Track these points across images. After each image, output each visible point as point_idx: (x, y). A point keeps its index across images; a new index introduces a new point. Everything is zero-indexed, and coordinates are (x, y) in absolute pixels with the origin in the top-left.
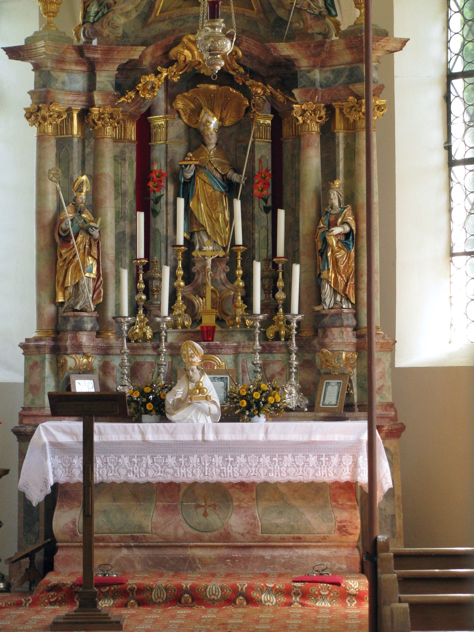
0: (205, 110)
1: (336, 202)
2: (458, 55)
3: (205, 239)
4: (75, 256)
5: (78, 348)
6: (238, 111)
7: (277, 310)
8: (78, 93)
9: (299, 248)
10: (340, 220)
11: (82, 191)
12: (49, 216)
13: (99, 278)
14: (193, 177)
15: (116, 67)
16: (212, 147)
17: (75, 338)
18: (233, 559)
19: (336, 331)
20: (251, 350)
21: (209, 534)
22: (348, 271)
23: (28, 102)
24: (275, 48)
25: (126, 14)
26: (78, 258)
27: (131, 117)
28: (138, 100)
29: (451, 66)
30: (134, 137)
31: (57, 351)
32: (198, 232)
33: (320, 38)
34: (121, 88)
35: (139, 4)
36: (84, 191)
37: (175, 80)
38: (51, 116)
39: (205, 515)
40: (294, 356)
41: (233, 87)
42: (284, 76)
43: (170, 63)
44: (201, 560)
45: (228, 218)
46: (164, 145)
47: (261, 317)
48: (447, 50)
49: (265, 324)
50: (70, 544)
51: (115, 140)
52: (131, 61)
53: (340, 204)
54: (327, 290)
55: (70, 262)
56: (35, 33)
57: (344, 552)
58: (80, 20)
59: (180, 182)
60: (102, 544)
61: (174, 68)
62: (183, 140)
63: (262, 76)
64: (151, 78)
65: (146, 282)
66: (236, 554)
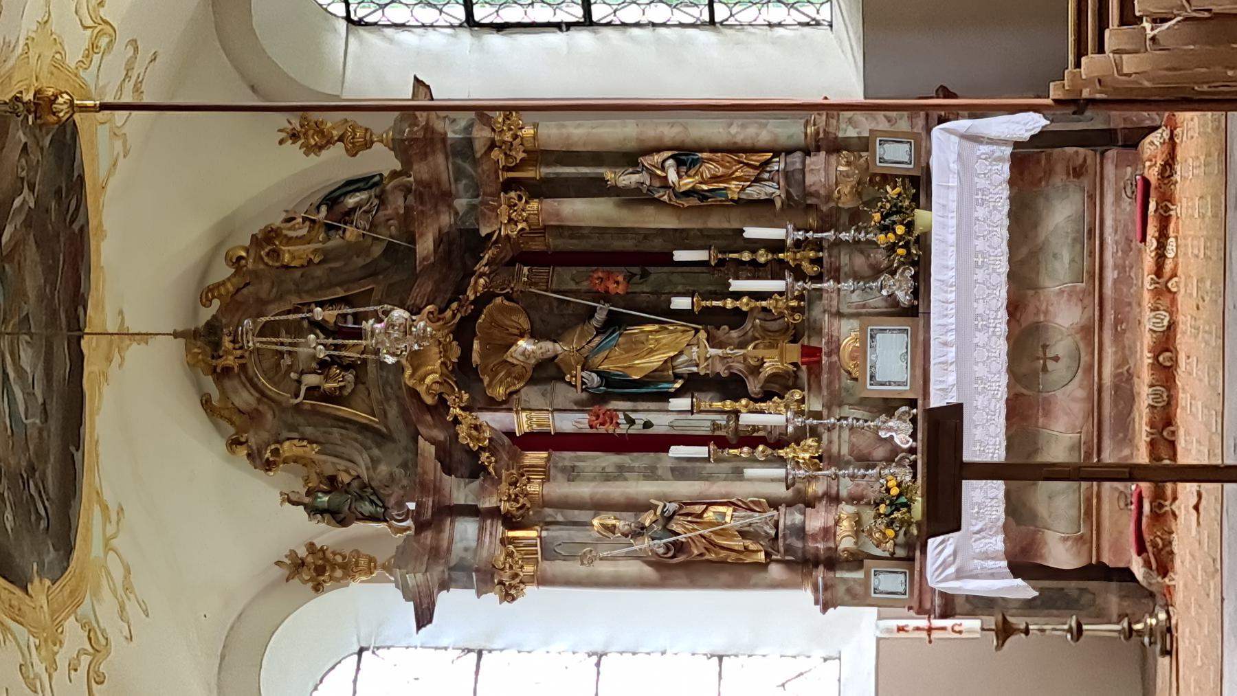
0: (508, 357)
1: (635, 178)
2: (441, 11)
3: (683, 358)
4: (702, 536)
5: (828, 533)
6: (510, 311)
7: (781, 261)
8: (481, 530)
9: (699, 230)
10: (659, 172)
11: (614, 526)
12: (648, 571)
13: (733, 504)
14: (599, 373)
15: (445, 476)
16: (558, 347)
17: (814, 537)
18: (1117, 322)
19: (810, 179)
20: (834, 295)
21: (1083, 354)
22: (651, 390)
23: (492, 598)
24: (424, 259)
25: (375, 462)
26: (705, 532)
28: (492, 448)
29: (456, 22)
30: (544, 454)
31: (832, 562)
32: (674, 368)
33: (411, 198)
34: (476, 471)
35: (361, 444)
36: (614, 522)
37: (466, 397)
38: (511, 567)
39: (1056, 359)
40: (844, 236)
41: (478, 317)
42: (463, 246)
43: (442, 403)
44: (1118, 366)
45: (656, 327)
46: (556, 414)
47: (789, 280)
48: (367, 24)
49: (799, 275)
50: (1094, 545)
51: (547, 479)
52: (438, 457)
53: (638, 172)
54: (755, 192)
55: (711, 542)
56: (397, 587)
57: (1110, 169)
58: (383, 525)
59: (606, 392)
60: (1095, 501)
61: (450, 399)
62: (549, 387)
63: (463, 278)
64: (462, 431)
65: (738, 445)
66: (1109, 317)
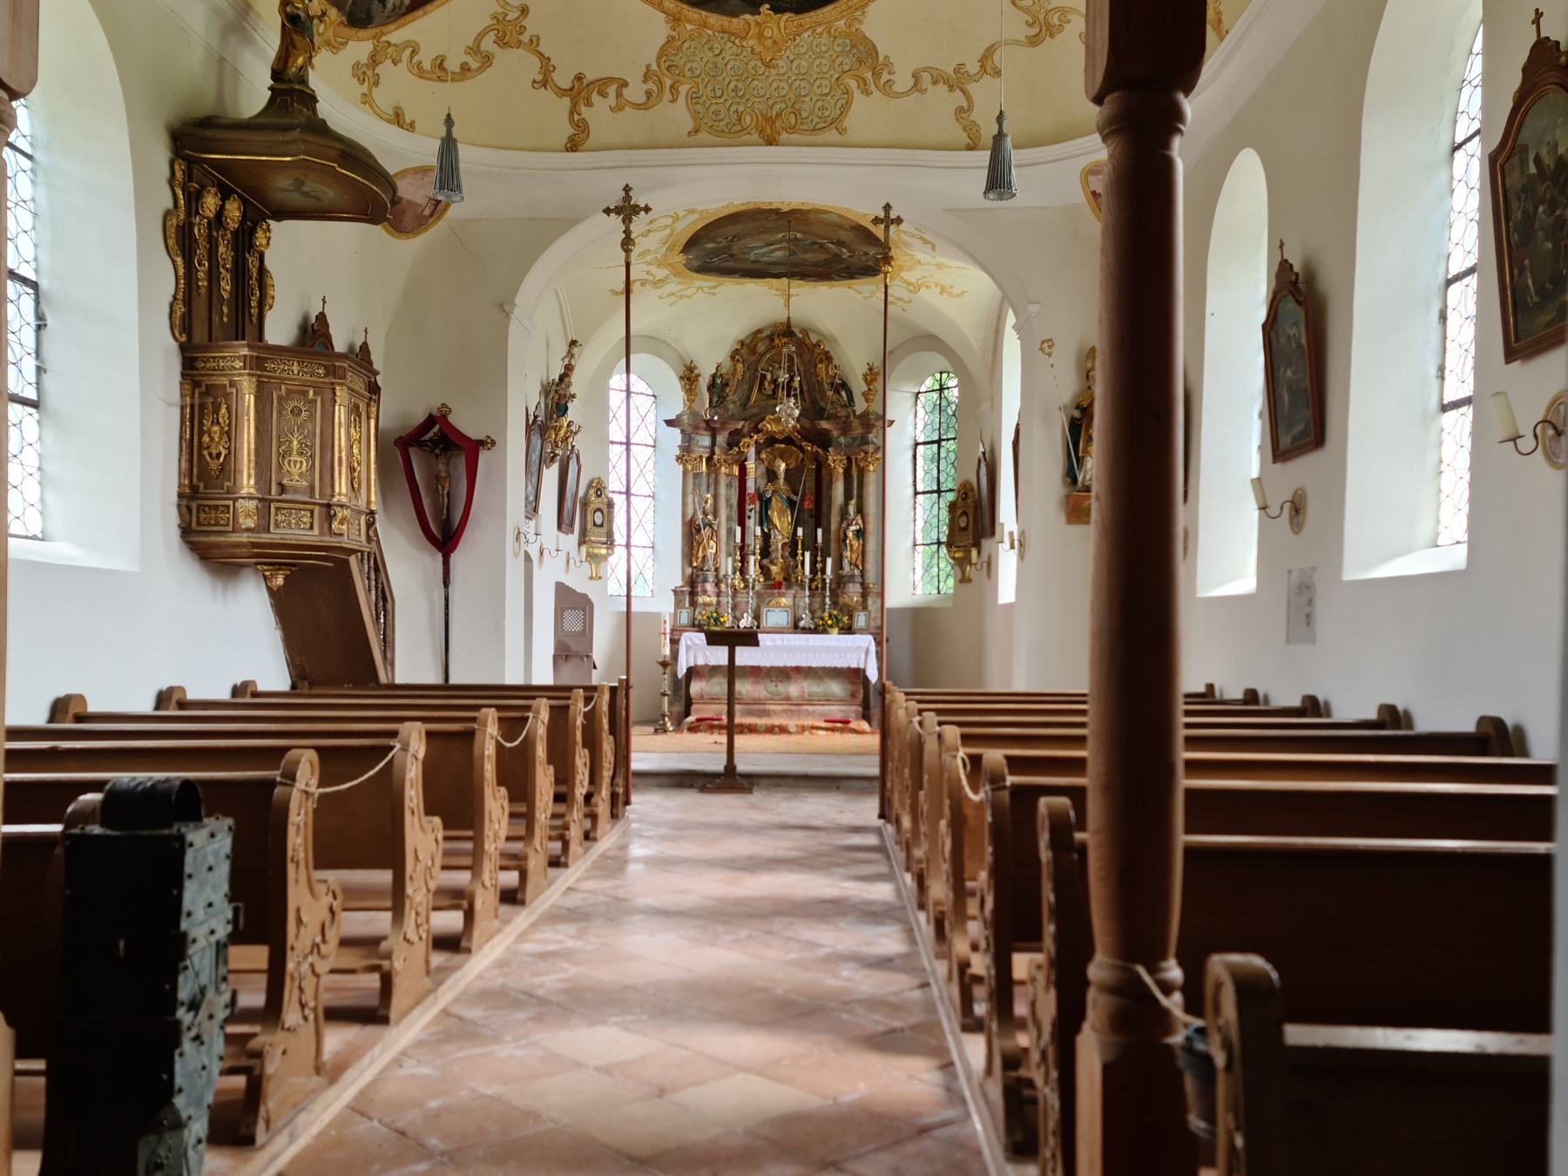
5: (705, 592)
23: (678, 452)
27: (736, 462)
28: (740, 452)
31: (693, 594)
34: (731, 445)
42: (824, 440)
43: (758, 431)
49: (812, 580)
54: (846, 562)
